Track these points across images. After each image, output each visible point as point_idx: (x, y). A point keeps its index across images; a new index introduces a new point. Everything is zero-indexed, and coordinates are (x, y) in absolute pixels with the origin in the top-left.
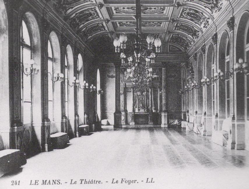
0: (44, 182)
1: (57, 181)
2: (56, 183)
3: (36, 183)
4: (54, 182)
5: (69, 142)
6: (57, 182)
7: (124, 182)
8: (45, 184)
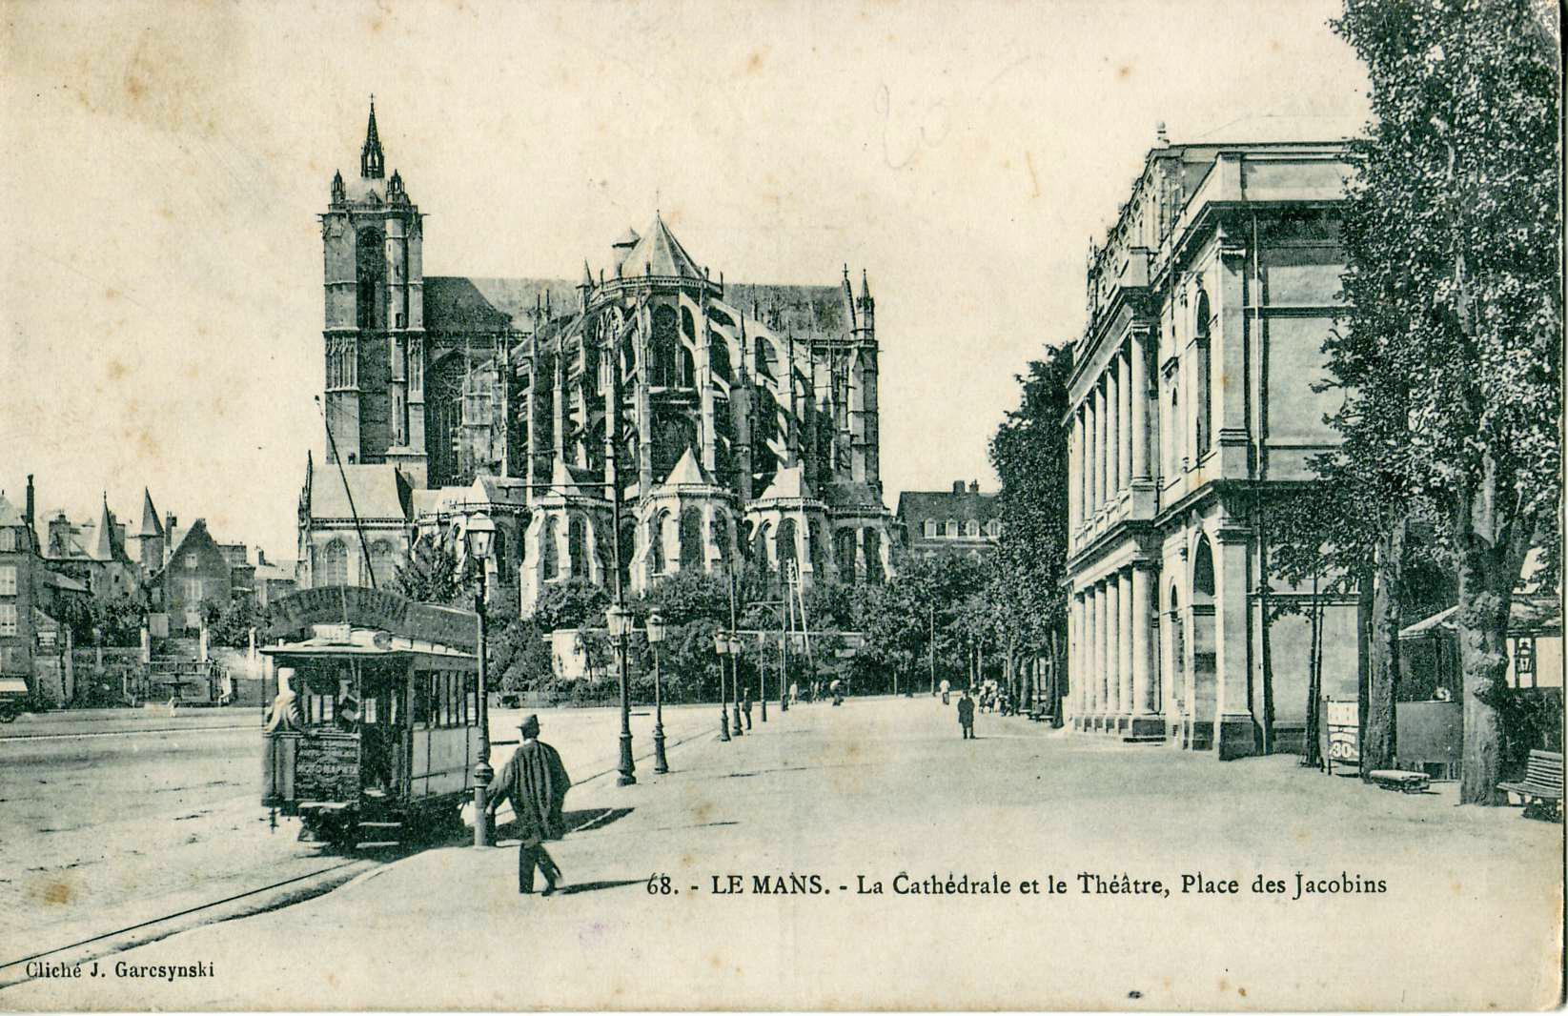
0: (761, 885)
1: (808, 880)
2: (807, 890)
3: (735, 887)
4: (796, 886)
5: (304, 821)
6: (808, 885)
7: (1193, 889)
8: (764, 889)
